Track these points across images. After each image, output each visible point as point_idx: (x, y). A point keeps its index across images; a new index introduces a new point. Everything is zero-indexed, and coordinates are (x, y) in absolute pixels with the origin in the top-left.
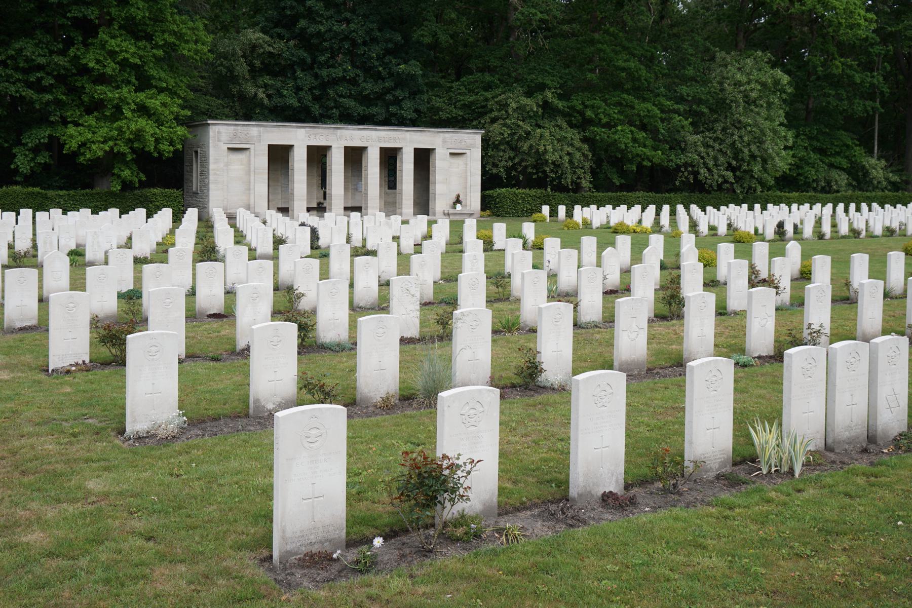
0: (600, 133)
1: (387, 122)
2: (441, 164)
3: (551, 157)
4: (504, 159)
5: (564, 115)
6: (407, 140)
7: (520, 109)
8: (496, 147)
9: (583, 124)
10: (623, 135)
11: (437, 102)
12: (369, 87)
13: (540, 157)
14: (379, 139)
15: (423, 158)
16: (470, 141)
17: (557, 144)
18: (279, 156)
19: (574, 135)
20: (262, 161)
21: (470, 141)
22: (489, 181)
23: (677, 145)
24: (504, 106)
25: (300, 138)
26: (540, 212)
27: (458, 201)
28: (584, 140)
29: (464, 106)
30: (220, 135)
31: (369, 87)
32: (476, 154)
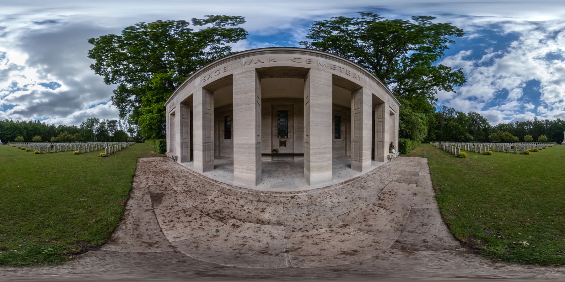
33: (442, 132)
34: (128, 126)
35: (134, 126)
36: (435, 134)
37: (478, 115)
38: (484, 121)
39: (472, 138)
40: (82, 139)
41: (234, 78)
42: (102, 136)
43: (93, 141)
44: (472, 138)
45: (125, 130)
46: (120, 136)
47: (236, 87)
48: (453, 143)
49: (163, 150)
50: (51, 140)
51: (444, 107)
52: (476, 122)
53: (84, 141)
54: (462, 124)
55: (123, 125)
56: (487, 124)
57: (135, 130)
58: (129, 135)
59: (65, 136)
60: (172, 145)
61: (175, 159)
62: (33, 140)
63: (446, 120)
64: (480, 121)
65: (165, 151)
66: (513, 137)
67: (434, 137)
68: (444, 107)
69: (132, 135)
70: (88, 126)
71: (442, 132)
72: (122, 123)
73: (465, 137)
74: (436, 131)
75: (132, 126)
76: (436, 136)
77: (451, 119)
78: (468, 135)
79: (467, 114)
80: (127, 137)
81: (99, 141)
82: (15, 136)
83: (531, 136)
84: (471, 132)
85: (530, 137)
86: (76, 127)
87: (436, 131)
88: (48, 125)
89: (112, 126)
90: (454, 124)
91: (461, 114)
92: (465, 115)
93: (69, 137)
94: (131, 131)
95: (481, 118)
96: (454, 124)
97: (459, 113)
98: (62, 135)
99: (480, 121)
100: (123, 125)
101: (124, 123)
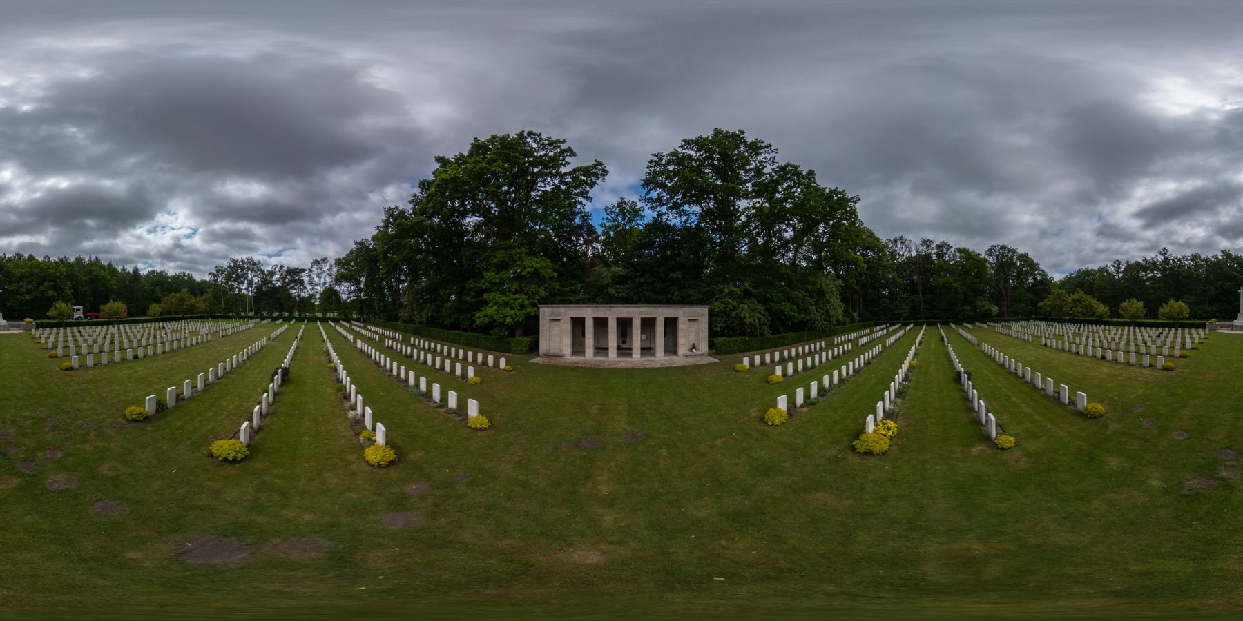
0: (775, 306)
1: (669, 302)
2: (682, 326)
3: (748, 320)
4: (720, 326)
5: (755, 296)
6: (660, 313)
7: (731, 293)
8: (717, 316)
9: (764, 301)
10: (787, 307)
11: (691, 292)
12: (658, 286)
13: (742, 320)
14: (641, 313)
15: (671, 324)
16: (702, 312)
17: (750, 313)
18: (578, 324)
19: (760, 307)
20: (567, 326)
21: (702, 312)
22: (712, 334)
23: (806, 311)
24: (721, 291)
25: (589, 313)
26: (775, 406)
27: (694, 347)
28: (766, 310)
29: (486, 303)
30: (545, 312)
31: (658, 286)
32: (704, 321)
44: (995, 309)
67: (905, 311)
82: (50, 302)
86: (190, 278)
97: (959, 251)
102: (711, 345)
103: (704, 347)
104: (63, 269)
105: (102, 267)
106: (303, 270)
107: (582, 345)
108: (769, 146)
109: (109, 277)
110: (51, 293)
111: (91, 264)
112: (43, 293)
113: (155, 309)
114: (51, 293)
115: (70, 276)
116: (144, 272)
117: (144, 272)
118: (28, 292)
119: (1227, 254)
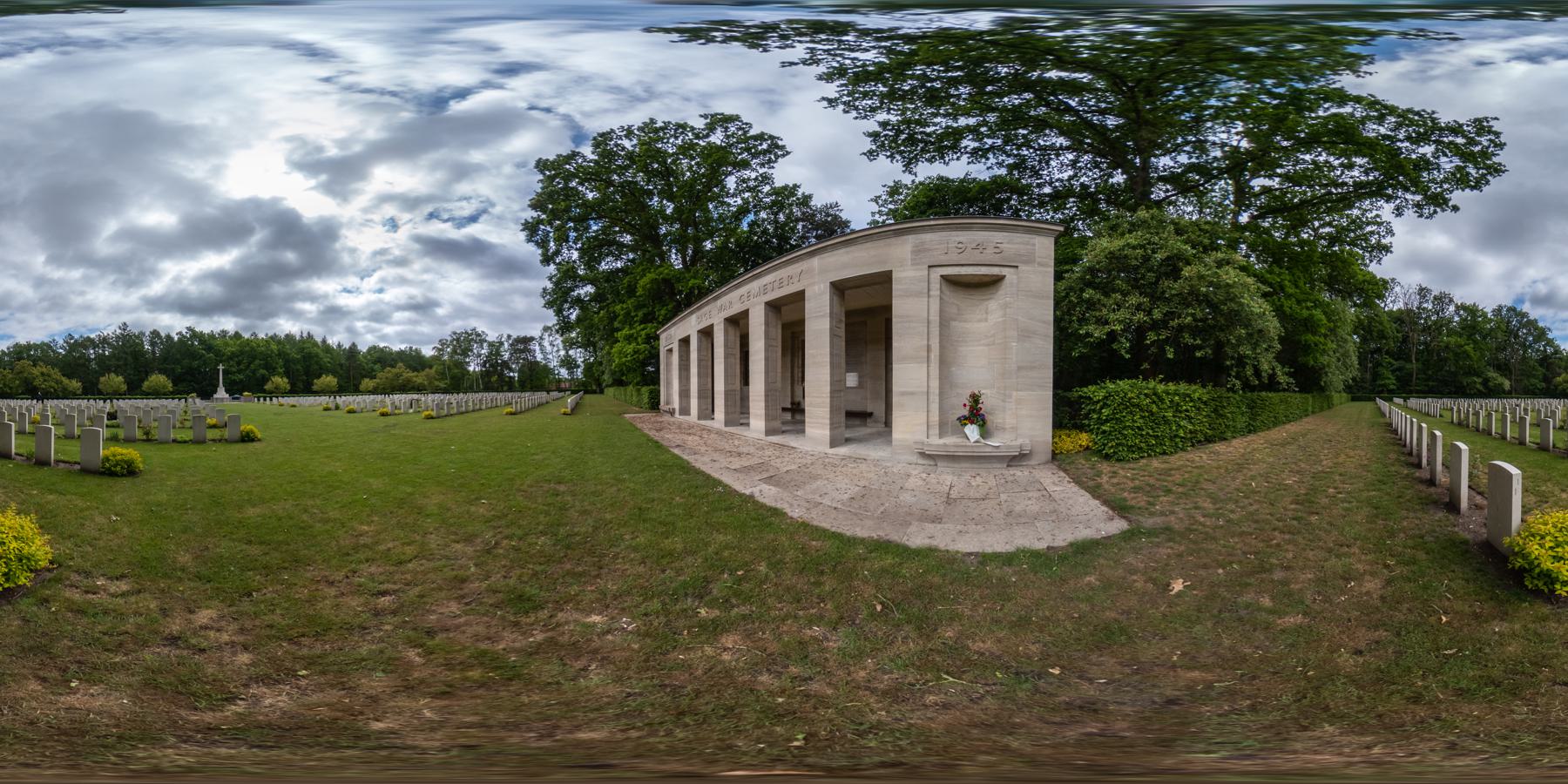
33: (1414, 366)
34: (562, 353)
35: (578, 355)
36: (1393, 371)
37: (1524, 315)
38: (1541, 334)
39: (1507, 384)
40: (442, 385)
41: (807, 294)
42: (494, 378)
43: (470, 389)
44: (1507, 384)
45: (554, 363)
46: (536, 378)
47: (809, 306)
48: (1448, 402)
49: (654, 405)
50: (362, 387)
51: (1421, 289)
52: (1517, 336)
53: (445, 391)
54: (1475, 342)
55: (549, 348)
56: (1550, 342)
57: (580, 361)
58: (564, 372)
59: (398, 376)
60: (669, 395)
61: (672, 413)
62: (315, 388)
63: (1426, 329)
64: (1529, 333)
65: (658, 403)
66: (65, 380)
67: (1391, 381)
68: (1421, 289)
69: (571, 373)
70: (454, 351)
71: (1414, 366)
72: (546, 344)
73: (1486, 382)
74: (1397, 364)
75: (571, 352)
76: (1398, 379)
77: (1442, 324)
78: (1492, 374)
79: (1489, 310)
80: (560, 381)
81: (488, 389)
82: (265, 380)
83: (121, 378)
84: (1504, 368)
85: (117, 380)
86: (418, 352)
87: (1397, 364)
88: (339, 345)
89: (522, 351)
90: (1452, 340)
91: (1472, 311)
92: (1484, 315)
93: (409, 381)
94: (568, 363)
95: (1532, 324)
96: (1452, 340)
97: (1464, 307)
98: (384, 375)
99: (1529, 333)
100: (551, 351)
101: (552, 344)
102: (1067, 414)
103: (1026, 416)
104: (274, 347)
105: (315, 344)
106: (532, 339)
107: (744, 400)
108: (1497, 134)
109: (322, 354)
110: (263, 371)
111: (302, 340)
112: (254, 372)
113: (367, 383)
114: (263, 371)
115: (280, 354)
116: (363, 348)
117: (363, 348)
118: (239, 372)
119: (940, 178)
